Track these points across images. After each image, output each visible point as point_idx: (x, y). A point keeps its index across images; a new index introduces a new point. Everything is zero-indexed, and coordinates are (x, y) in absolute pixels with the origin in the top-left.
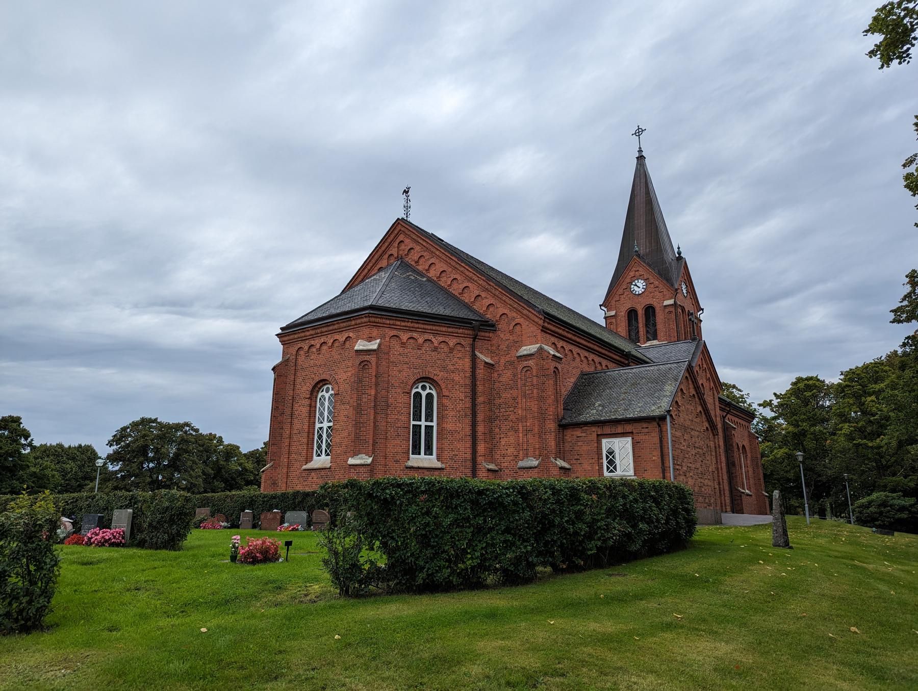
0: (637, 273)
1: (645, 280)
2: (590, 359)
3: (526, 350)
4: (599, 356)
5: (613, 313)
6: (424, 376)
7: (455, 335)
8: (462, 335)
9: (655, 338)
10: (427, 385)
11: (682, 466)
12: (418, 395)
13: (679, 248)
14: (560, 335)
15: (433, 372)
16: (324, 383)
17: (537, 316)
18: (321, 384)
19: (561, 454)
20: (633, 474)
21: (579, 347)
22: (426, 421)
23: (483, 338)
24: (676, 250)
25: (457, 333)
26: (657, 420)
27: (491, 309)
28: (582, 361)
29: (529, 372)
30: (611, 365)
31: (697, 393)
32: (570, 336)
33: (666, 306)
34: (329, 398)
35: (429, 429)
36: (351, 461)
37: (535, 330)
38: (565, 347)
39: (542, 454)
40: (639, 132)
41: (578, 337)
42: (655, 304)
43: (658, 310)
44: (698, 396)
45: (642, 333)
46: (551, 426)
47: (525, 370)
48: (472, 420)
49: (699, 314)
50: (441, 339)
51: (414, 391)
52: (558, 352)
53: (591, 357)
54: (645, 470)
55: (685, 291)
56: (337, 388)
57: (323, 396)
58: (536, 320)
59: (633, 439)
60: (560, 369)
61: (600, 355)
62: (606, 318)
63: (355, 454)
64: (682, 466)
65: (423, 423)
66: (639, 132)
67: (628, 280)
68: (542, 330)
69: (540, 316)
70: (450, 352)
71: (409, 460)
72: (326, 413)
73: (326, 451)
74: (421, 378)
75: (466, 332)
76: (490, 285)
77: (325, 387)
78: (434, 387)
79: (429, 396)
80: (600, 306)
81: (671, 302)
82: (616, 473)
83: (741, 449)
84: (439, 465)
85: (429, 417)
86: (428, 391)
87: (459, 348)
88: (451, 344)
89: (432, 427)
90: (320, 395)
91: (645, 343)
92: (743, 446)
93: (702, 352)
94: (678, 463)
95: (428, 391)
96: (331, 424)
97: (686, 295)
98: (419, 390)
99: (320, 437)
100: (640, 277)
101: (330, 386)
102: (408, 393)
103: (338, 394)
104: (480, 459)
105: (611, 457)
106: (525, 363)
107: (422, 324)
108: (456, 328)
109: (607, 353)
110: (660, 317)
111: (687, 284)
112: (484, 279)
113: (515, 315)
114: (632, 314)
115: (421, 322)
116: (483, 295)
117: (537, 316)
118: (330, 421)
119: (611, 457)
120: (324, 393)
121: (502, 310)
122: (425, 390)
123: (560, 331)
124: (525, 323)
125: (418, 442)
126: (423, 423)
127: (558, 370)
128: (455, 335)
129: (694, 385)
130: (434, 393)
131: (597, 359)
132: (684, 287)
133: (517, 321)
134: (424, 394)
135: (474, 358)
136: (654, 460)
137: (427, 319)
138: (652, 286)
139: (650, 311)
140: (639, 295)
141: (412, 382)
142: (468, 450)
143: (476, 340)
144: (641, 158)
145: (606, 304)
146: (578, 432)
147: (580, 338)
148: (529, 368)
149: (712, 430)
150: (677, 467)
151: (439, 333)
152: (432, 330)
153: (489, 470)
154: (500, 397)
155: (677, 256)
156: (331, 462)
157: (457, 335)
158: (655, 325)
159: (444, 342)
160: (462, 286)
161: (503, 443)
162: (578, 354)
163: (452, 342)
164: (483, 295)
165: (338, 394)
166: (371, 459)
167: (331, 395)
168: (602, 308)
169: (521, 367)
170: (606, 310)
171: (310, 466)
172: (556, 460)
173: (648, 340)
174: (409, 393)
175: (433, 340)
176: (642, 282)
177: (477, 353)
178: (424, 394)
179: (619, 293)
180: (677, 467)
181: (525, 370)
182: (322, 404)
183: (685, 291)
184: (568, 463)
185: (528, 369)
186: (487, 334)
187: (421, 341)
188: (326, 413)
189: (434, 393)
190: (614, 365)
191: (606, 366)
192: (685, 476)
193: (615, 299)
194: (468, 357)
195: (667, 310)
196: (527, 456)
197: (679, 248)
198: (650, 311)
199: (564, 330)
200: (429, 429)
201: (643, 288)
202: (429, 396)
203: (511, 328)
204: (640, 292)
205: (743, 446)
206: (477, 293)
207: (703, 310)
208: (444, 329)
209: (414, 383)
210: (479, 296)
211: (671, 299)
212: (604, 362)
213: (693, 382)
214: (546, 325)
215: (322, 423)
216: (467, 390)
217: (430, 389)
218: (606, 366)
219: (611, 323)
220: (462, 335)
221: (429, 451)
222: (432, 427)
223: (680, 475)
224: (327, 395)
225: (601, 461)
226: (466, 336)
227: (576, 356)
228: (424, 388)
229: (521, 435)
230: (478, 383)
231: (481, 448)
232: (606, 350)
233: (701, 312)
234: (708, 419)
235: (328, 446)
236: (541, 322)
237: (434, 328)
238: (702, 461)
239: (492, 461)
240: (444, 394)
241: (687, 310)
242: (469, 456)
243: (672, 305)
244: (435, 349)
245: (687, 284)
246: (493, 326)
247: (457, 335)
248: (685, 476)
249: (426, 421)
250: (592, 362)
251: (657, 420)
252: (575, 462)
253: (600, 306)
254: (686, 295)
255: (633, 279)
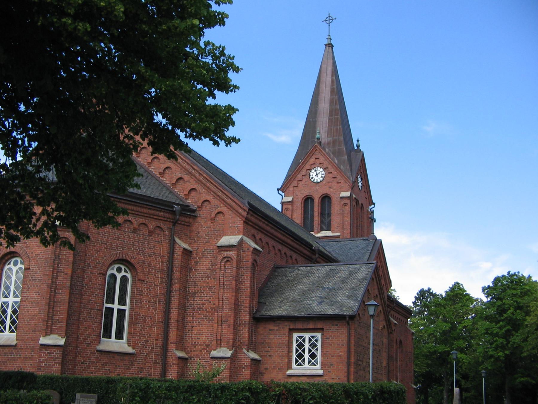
0: (317, 160)
1: (325, 169)
2: (283, 252)
3: (225, 240)
4: (291, 249)
5: (289, 199)
6: (121, 258)
7: (155, 217)
8: (163, 219)
9: (329, 229)
10: (123, 267)
11: (362, 361)
12: (113, 277)
13: (358, 141)
14: (260, 227)
15: (130, 255)
16: (12, 255)
17: (241, 207)
18: (9, 256)
19: (252, 347)
20: (320, 368)
21: (274, 240)
22: (119, 304)
23: (182, 223)
24: (355, 143)
25: (158, 216)
26: (347, 319)
27: (193, 194)
28: (276, 254)
29: (228, 263)
30: (300, 258)
31: (380, 294)
32: (268, 228)
33: (342, 198)
34: (17, 272)
35: (121, 313)
36: (44, 341)
37: (239, 223)
38: (263, 239)
39: (235, 345)
40: (329, 20)
41: (276, 230)
42: (332, 195)
43: (334, 201)
44: (380, 297)
45: (317, 222)
46: (245, 318)
47: (225, 260)
48: (166, 306)
49: (370, 207)
50: (141, 220)
51: (109, 272)
52: (257, 243)
53: (284, 250)
54: (331, 365)
55: (360, 184)
56: (27, 263)
57: (10, 269)
58: (240, 211)
59: (322, 334)
60: (258, 262)
61: (293, 249)
62: (283, 203)
63: (48, 332)
64: (362, 361)
65: (116, 306)
66: (329, 20)
67: (307, 167)
68: (244, 222)
69: (245, 208)
70: (148, 235)
71: (100, 343)
72: (12, 288)
73: (10, 327)
74: (117, 260)
75: (167, 215)
76: (195, 169)
77: (13, 260)
78: (130, 270)
79: (124, 279)
80: (278, 190)
81: (348, 194)
82: (304, 366)
83: (398, 344)
84: (130, 350)
85: (122, 301)
86: (123, 273)
87: (158, 231)
88: (151, 227)
89: (125, 310)
90: (6, 267)
91: (318, 233)
92: (401, 341)
93: (378, 251)
94: (361, 359)
95: (123, 273)
96: (18, 300)
97: (361, 188)
98: (115, 272)
99: (313, 356)
100: (321, 165)
101: (19, 260)
102: (103, 274)
103: (29, 269)
104: (171, 347)
105: (300, 351)
106: (226, 254)
107: (124, 203)
108: (157, 210)
109: (298, 247)
110: (336, 208)
111: (363, 178)
112: (189, 162)
113: (217, 202)
114: (308, 200)
115: (123, 201)
116: (186, 177)
117: (241, 207)
118: (17, 296)
119: (300, 351)
120: (11, 266)
121: (204, 197)
122: (120, 273)
123: (260, 224)
124: (229, 213)
125: (109, 325)
126: (116, 306)
127: (257, 263)
128: (155, 217)
129: (378, 286)
130: (129, 276)
131: (289, 253)
132: (360, 180)
133: (220, 209)
134: (119, 276)
135: (173, 244)
136: (340, 356)
137: (143, 202)
138: (331, 175)
139: (326, 199)
140: (317, 183)
141: (108, 263)
142: (160, 336)
143: (176, 225)
144: (330, 46)
145: (284, 189)
146: (271, 326)
147: (277, 231)
148: (229, 259)
149: (387, 328)
150: (360, 363)
151: (140, 214)
152: (133, 210)
153: (180, 358)
154: (195, 286)
155: (356, 148)
156: (17, 340)
157: (157, 217)
158: (329, 215)
159: (144, 224)
160: (163, 167)
161: (195, 332)
162: (273, 247)
163: (152, 225)
164: (186, 177)
165: (29, 269)
166: (64, 340)
167: (20, 269)
168: (280, 192)
169: (221, 256)
170: (283, 194)
171: (289, 372)
172: (248, 351)
173: (322, 229)
174: (105, 275)
175: (133, 221)
176: (322, 170)
177: (178, 240)
178: (119, 276)
179: (297, 179)
180: (360, 363)
181: (225, 260)
182: (9, 277)
183: (360, 184)
184: (259, 355)
185: (228, 259)
186: (187, 220)
187: (136, 224)
188: (12, 288)
189: (129, 276)
190: (303, 259)
191: (296, 260)
192: (364, 370)
193: (293, 185)
194: (167, 241)
195: (343, 202)
196: (219, 346)
197: (358, 141)
198: (326, 199)
199: (264, 223)
200: (121, 313)
201: (321, 177)
202: (124, 279)
203: (213, 216)
204: (319, 181)
205: (401, 341)
206: (179, 175)
207: (374, 204)
208: (145, 211)
209: (111, 265)
210: (180, 178)
211: (347, 191)
212: (295, 256)
213: (377, 283)
214: (249, 216)
215: (8, 297)
216: (164, 276)
217: (126, 271)
218: (296, 260)
219: (287, 209)
220: (163, 219)
221: (119, 336)
222: (125, 310)
223: (360, 369)
224: (15, 269)
225: (290, 354)
226: (166, 219)
227: (271, 248)
228: (119, 270)
229: (216, 325)
230: (175, 269)
231: (173, 335)
232: (298, 244)
233: (373, 206)
234: (385, 318)
235: (13, 322)
236: (245, 214)
237: (135, 208)
238: (378, 357)
239: (181, 349)
240: (139, 278)
241: (360, 203)
242: (160, 343)
243: (348, 197)
244: (135, 230)
245: (363, 178)
246: (194, 211)
247: (157, 217)
248: (364, 370)
249: (119, 304)
250: (284, 256)
251: (347, 319)
252: (265, 354)
253: (278, 190)
254: (361, 188)
255: (312, 166)
